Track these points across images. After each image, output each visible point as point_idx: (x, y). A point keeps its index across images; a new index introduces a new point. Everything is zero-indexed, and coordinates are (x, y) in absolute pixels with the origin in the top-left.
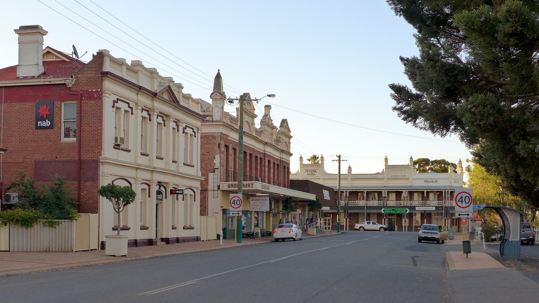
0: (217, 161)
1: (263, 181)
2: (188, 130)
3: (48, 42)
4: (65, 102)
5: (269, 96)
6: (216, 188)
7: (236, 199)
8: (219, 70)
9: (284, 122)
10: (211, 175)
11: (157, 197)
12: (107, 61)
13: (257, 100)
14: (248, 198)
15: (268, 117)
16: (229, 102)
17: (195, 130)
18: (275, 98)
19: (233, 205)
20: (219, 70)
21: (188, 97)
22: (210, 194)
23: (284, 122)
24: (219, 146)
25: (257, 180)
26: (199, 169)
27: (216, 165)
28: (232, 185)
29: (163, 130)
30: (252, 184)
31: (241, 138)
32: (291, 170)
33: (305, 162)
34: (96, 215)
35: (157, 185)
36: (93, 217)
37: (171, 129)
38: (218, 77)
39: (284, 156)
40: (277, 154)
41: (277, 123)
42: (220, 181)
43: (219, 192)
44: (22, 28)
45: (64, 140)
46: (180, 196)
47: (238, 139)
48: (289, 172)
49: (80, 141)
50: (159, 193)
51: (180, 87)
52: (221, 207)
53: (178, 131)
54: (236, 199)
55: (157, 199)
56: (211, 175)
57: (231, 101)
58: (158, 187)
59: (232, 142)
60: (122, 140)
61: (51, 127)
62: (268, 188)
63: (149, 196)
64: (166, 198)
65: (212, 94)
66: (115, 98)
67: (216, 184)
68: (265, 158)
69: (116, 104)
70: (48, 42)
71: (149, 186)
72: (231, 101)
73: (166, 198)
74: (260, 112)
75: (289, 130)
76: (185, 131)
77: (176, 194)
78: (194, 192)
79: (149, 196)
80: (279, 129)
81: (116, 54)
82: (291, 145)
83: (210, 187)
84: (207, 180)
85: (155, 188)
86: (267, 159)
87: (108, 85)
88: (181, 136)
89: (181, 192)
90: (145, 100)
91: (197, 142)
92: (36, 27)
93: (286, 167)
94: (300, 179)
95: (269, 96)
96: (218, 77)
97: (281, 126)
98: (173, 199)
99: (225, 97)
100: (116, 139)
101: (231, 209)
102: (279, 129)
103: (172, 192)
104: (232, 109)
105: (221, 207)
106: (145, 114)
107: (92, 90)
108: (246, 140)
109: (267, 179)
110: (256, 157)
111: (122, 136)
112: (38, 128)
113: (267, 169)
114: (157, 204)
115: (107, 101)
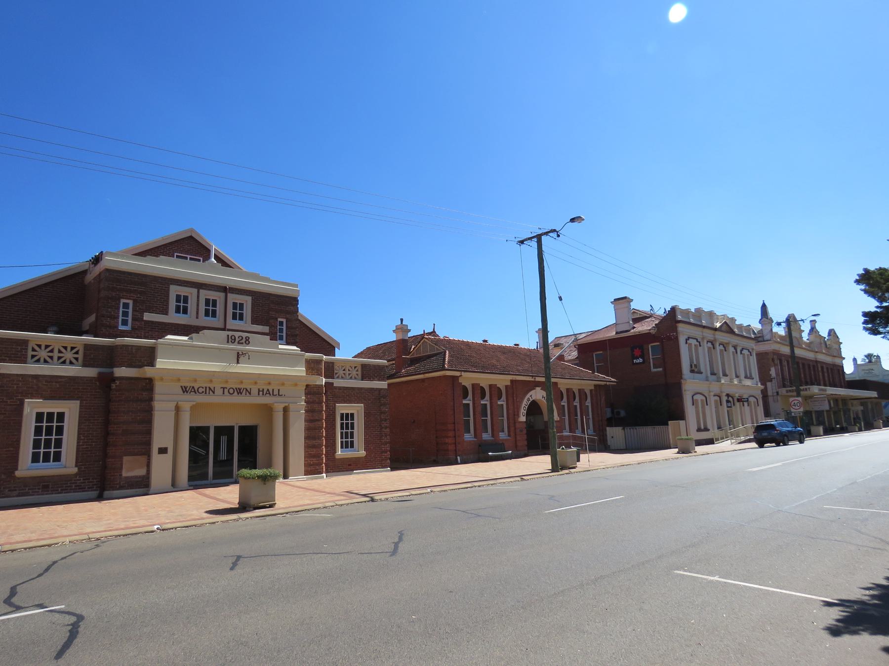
0: (773, 372)
1: (819, 384)
2: (745, 352)
3: (633, 305)
4: (596, 353)
5: (573, 220)
6: (775, 394)
7: (796, 402)
8: (764, 301)
9: (832, 333)
10: (769, 384)
11: (727, 405)
12: (678, 313)
13: (803, 320)
14: (806, 400)
15: (815, 330)
16: (777, 325)
17: (750, 350)
18: (820, 316)
19: (794, 407)
20: (764, 301)
21: (740, 327)
22: (771, 399)
23: (832, 333)
24: (773, 360)
25: (812, 384)
26: (758, 380)
27: (773, 376)
28: (790, 391)
29: (724, 354)
30: (809, 388)
31: (792, 351)
32: (845, 370)
33: (859, 362)
34: (684, 421)
35: (726, 396)
36: (682, 423)
37: (731, 354)
38: (764, 307)
39: (837, 361)
40: (828, 359)
41: (824, 333)
42: (778, 388)
43: (779, 398)
44: (615, 300)
45: (653, 370)
46: (746, 404)
47: (795, 348)
48: (844, 373)
49: (665, 370)
50: (728, 401)
51: (733, 320)
52: (783, 409)
53: (736, 353)
54: (796, 402)
55: (728, 407)
56: (769, 384)
57: (779, 324)
58: (726, 398)
59: (784, 355)
60: (695, 366)
61: (644, 362)
62: (825, 390)
63: (721, 405)
64: (734, 405)
65: (760, 320)
66: (686, 337)
67: (775, 391)
68: (817, 365)
69: (688, 341)
70: (633, 305)
71: (720, 397)
72: (779, 324)
73: (734, 405)
74: (806, 327)
75: (838, 337)
76: (743, 352)
77: (742, 401)
78: (757, 399)
79: (721, 405)
80: (827, 338)
81: (683, 306)
82: (842, 350)
83: (770, 393)
84: (766, 388)
85: (724, 399)
86: (819, 366)
87: (681, 327)
88: (740, 356)
89: (746, 400)
90: (709, 334)
91: (753, 360)
92: (625, 298)
93: (841, 368)
94: (857, 379)
95: (573, 220)
96: (764, 307)
97: (829, 334)
98: (740, 406)
99: (772, 321)
100: (691, 366)
101: (793, 410)
102: (827, 338)
103: (739, 400)
104: (781, 331)
105: (783, 409)
106: (710, 345)
107: (670, 335)
108: (798, 352)
109: (822, 383)
110: (809, 365)
111: (695, 363)
112: (634, 364)
113: (821, 374)
114: (728, 411)
115: (682, 340)
